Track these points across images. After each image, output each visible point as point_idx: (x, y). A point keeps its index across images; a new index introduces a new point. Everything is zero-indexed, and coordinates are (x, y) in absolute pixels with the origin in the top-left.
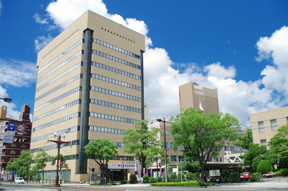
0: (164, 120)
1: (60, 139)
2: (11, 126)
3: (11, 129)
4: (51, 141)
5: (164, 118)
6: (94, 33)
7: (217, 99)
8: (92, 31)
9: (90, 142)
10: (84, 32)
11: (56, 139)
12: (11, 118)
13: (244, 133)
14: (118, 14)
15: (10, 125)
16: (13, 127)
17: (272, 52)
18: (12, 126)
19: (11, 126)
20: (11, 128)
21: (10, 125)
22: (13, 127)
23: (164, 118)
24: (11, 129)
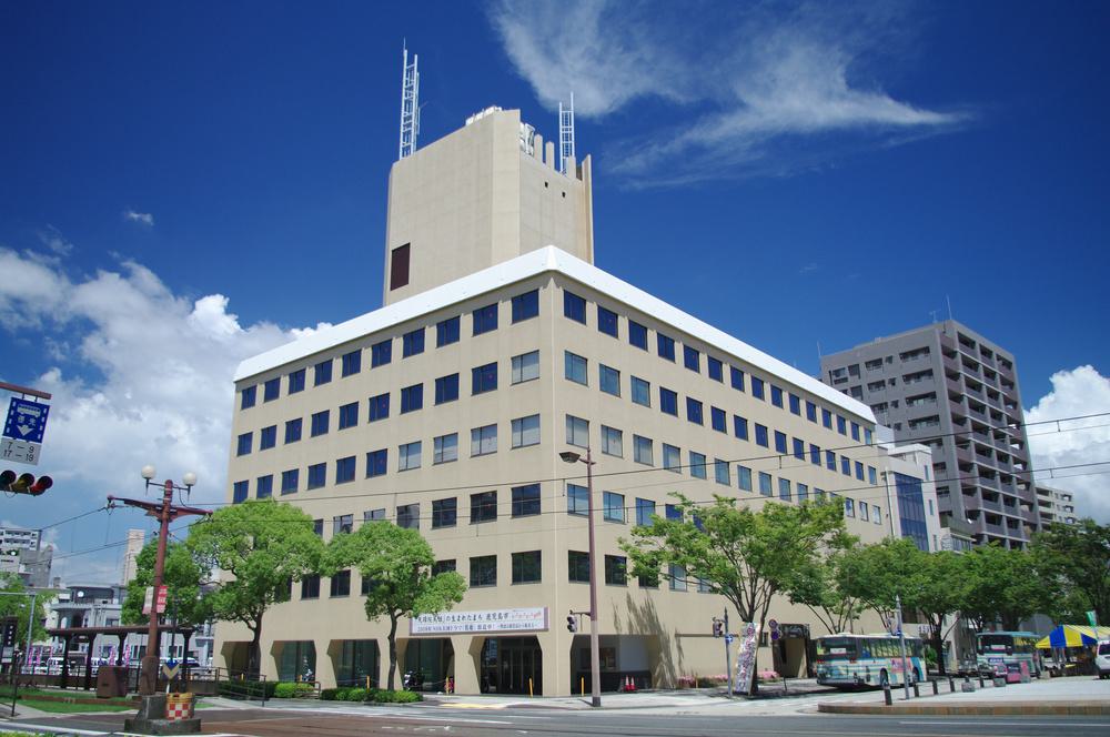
0: (589, 457)
1: (168, 494)
2: (22, 419)
3: (25, 430)
4: (127, 502)
5: (726, 611)
7: (238, 643)
9: (841, 81)
11: (155, 496)
12: (1037, 457)
13: (931, 560)
14: (326, 322)
15: (19, 410)
16: (32, 421)
17: (369, 620)
18: (28, 417)
19: (22, 419)
20: (25, 427)
21: (19, 410)
22: (32, 421)
23: (726, 611)
24: (25, 430)
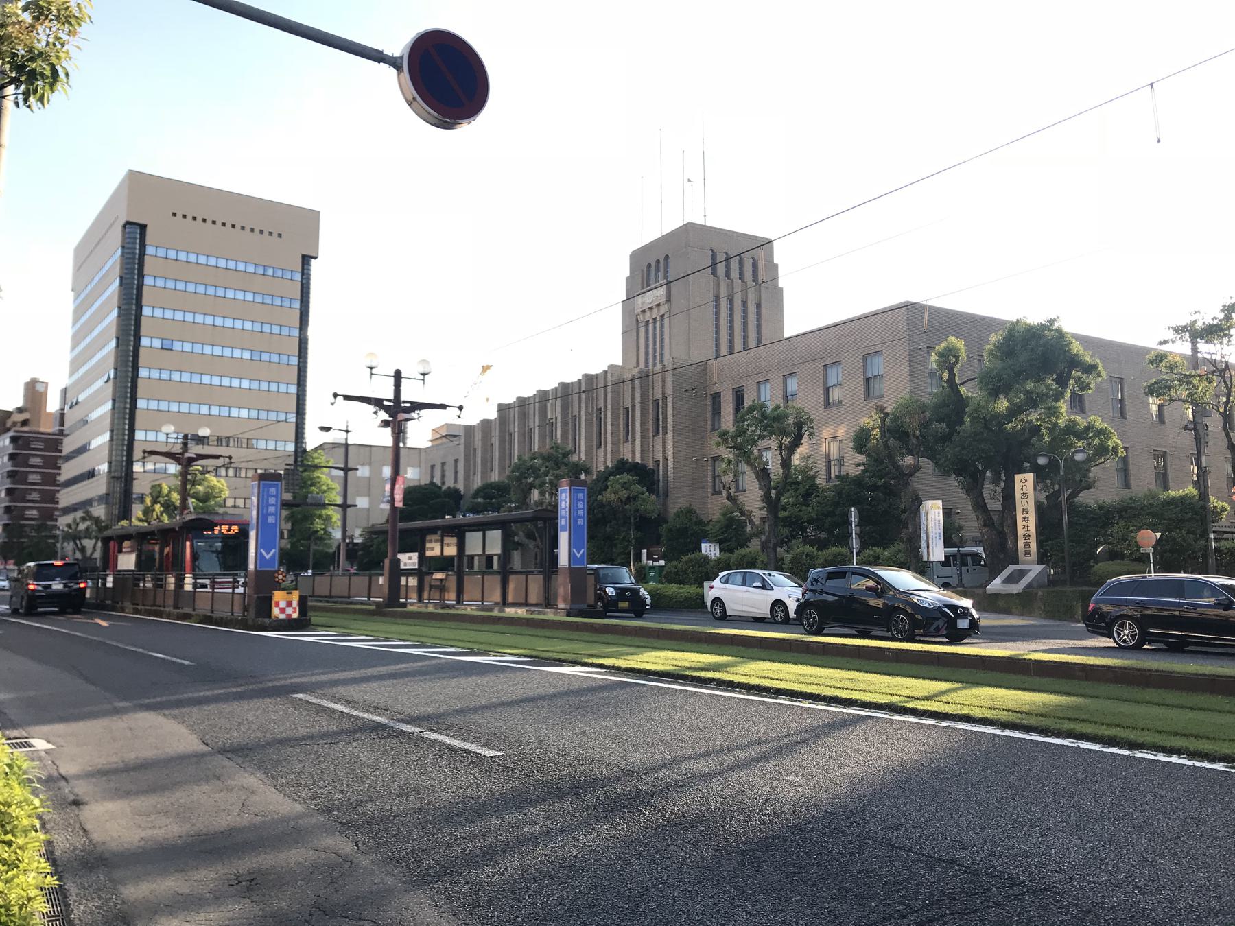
6: (149, 231)
8: (143, 227)
10: (124, 226)
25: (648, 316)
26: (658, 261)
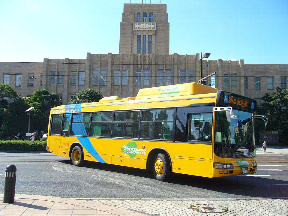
25: (139, 33)
26: (145, 13)
